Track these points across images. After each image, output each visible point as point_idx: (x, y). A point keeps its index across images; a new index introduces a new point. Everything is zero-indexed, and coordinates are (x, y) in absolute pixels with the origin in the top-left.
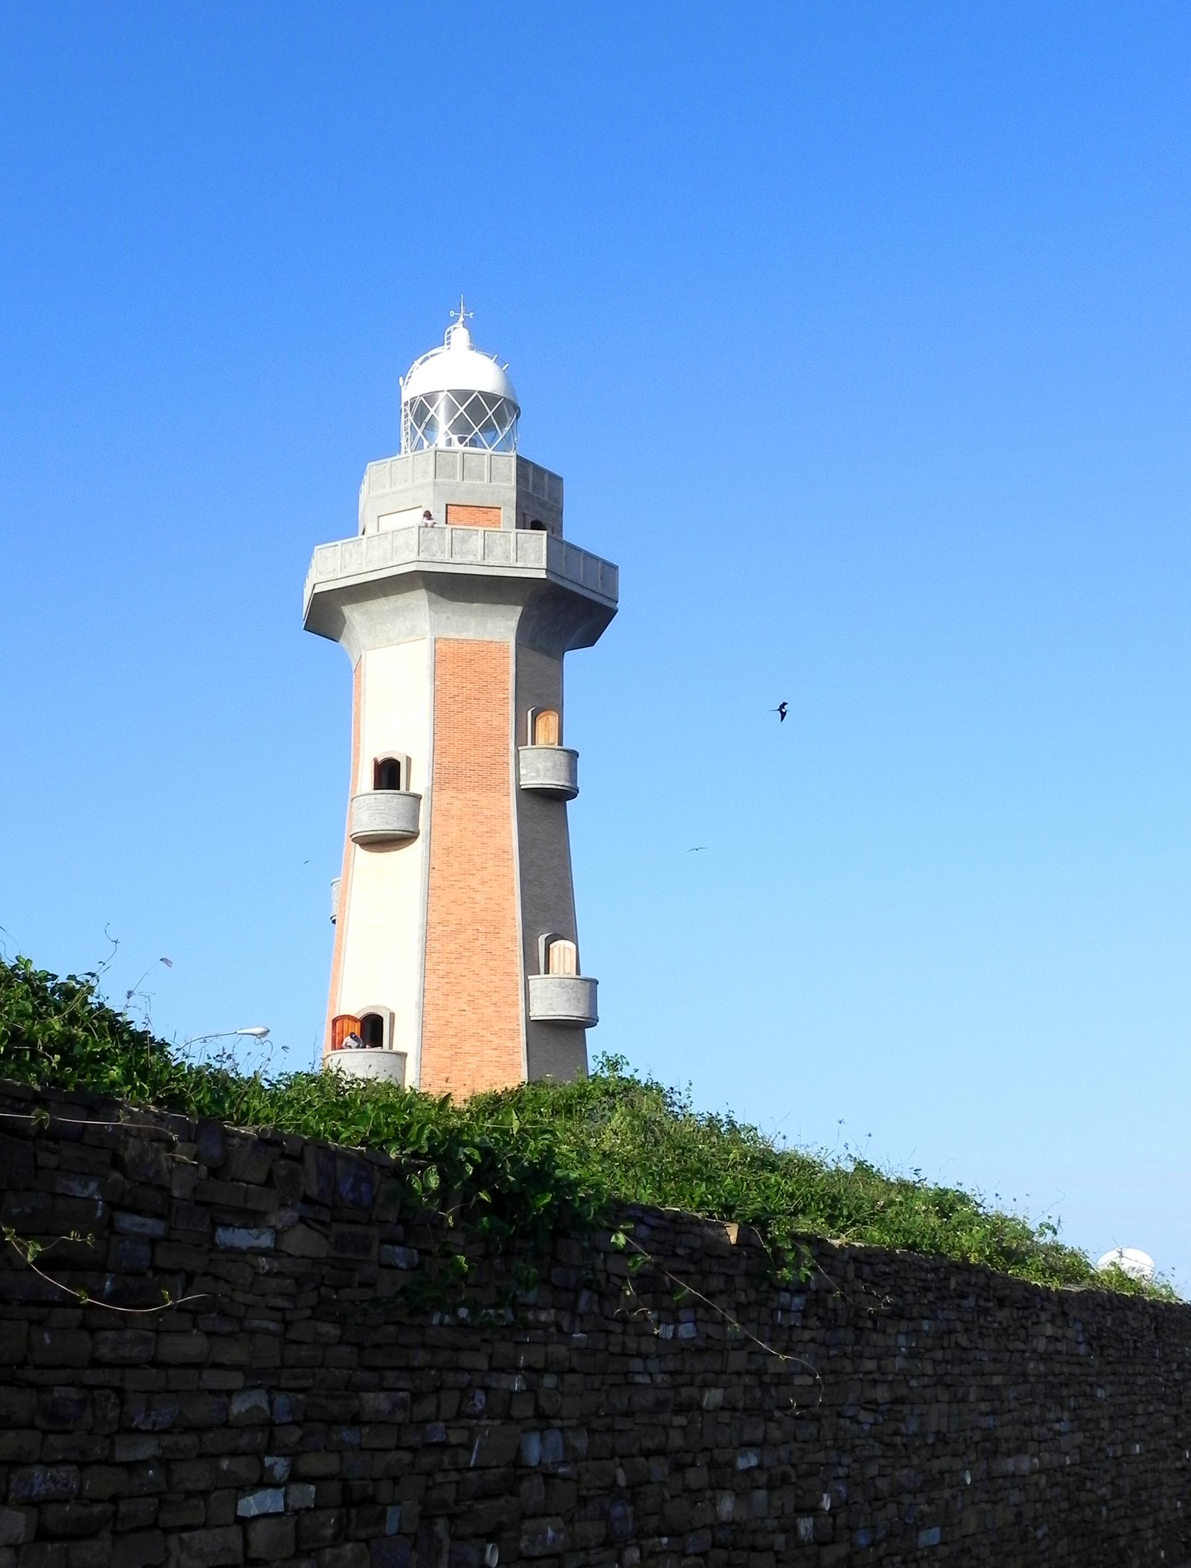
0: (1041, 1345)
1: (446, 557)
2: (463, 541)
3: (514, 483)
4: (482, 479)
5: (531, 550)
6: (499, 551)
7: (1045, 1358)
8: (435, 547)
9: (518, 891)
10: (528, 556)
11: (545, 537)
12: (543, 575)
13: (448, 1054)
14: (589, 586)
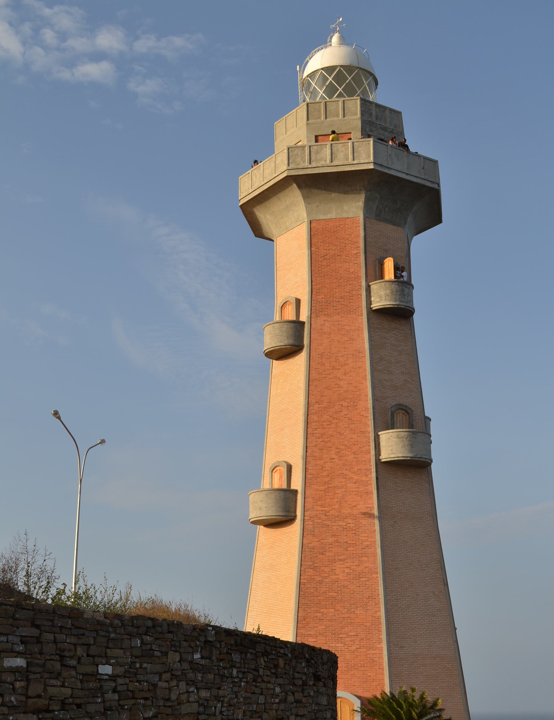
1: (306, 164)
2: (317, 152)
3: (359, 115)
4: (338, 116)
5: (362, 152)
6: (341, 155)
8: (299, 159)
9: (369, 377)
10: (361, 155)
11: (372, 142)
12: (371, 166)
13: (323, 488)
14: (355, 154)
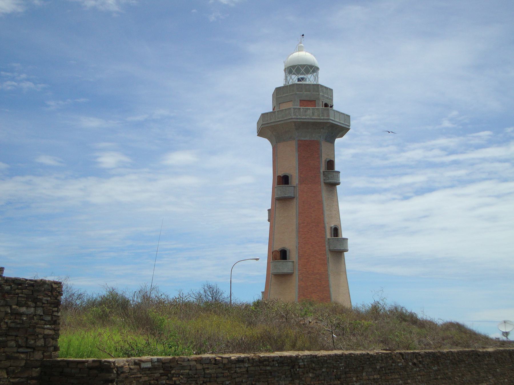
0: (486, 362)
6: (316, 114)
7: (486, 365)
